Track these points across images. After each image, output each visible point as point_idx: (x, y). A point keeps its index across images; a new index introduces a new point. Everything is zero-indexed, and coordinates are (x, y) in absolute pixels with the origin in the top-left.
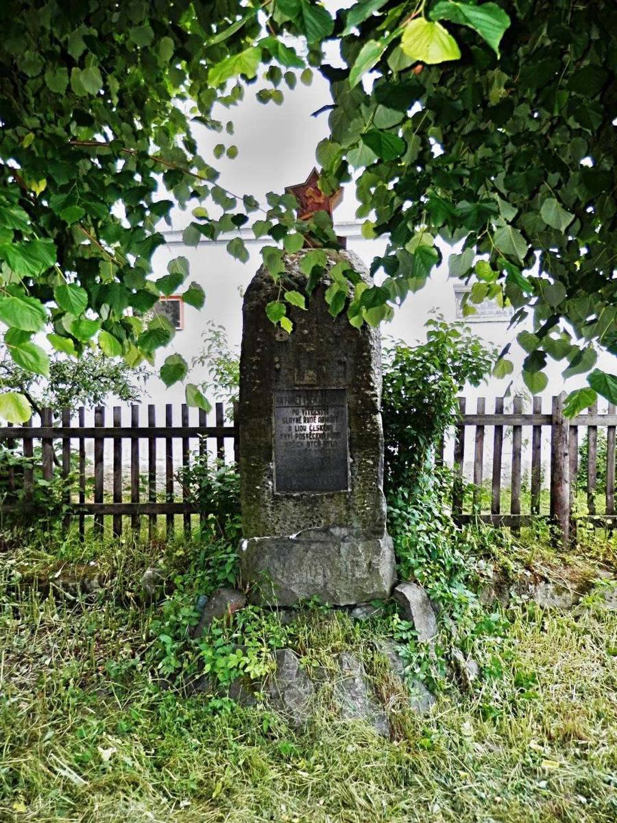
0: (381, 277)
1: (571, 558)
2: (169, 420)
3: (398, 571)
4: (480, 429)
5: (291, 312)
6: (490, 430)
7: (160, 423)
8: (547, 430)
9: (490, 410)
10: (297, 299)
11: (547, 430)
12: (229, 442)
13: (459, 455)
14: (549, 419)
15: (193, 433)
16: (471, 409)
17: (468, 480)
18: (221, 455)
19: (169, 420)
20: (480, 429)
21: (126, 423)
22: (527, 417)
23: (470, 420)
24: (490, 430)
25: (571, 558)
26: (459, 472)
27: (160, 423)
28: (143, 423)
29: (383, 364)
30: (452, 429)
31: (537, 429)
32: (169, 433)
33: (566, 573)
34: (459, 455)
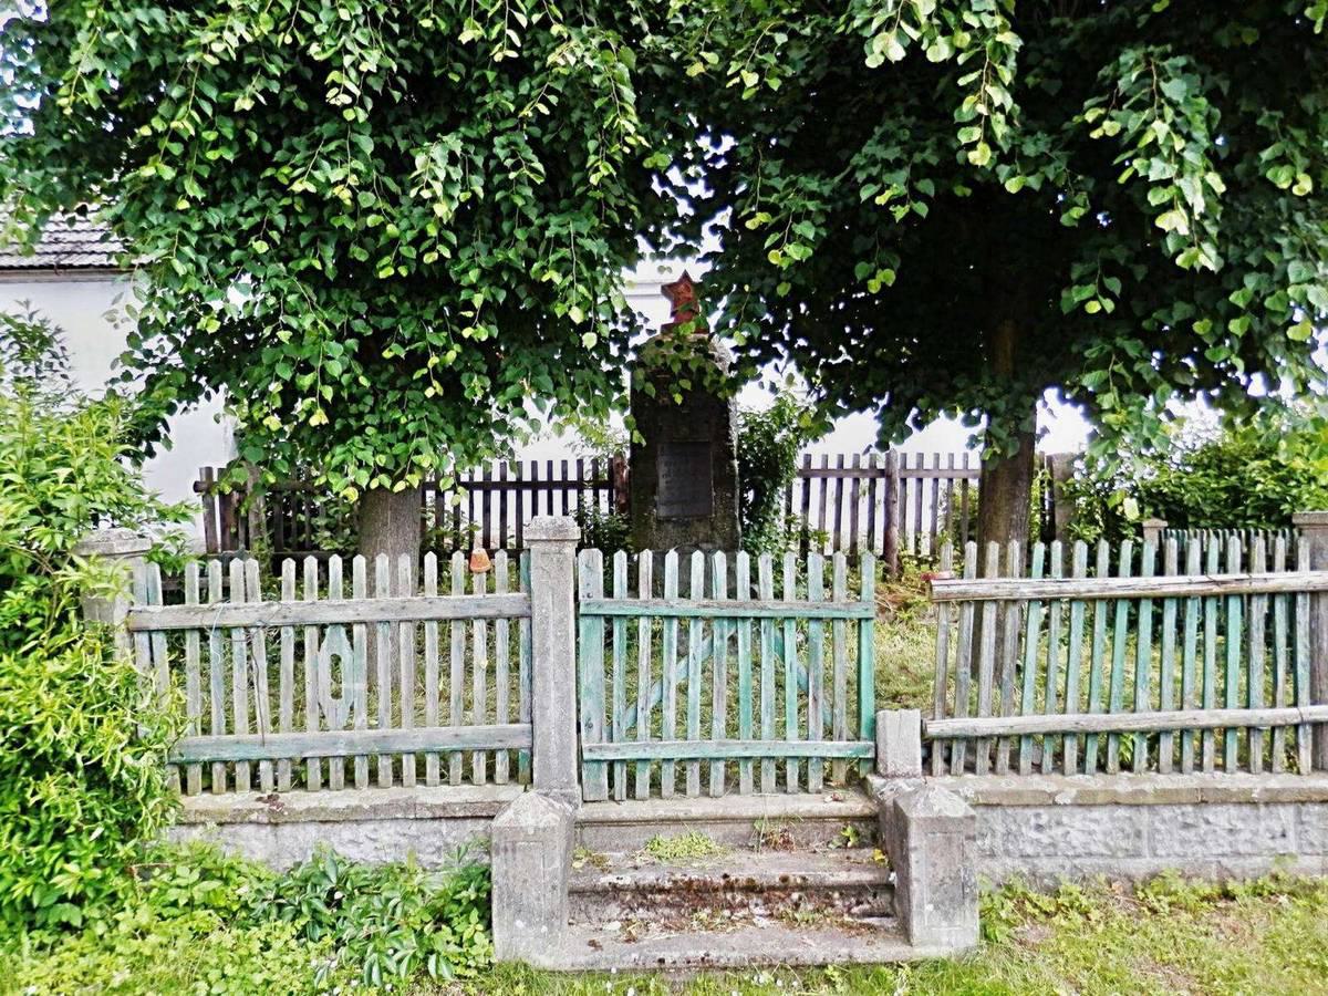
0: (733, 374)
1: (894, 586)
2: (565, 472)
3: (1058, 600)
4: (824, 481)
5: (683, 392)
6: (832, 483)
7: (557, 477)
8: (881, 482)
9: (833, 465)
10: (686, 384)
11: (881, 482)
12: (604, 493)
13: (806, 504)
14: (882, 473)
15: (512, 485)
16: (816, 464)
17: (813, 524)
18: (597, 503)
19: (565, 472)
20: (824, 481)
21: (572, 476)
22: (863, 471)
23: (816, 473)
24: (832, 483)
25: (894, 586)
26: (806, 519)
27: (572, 476)
28: (557, 477)
29: (737, 429)
30: (798, 482)
31: (873, 481)
32: (565, 485)
33: (890, 597)
34: (806, 504)
